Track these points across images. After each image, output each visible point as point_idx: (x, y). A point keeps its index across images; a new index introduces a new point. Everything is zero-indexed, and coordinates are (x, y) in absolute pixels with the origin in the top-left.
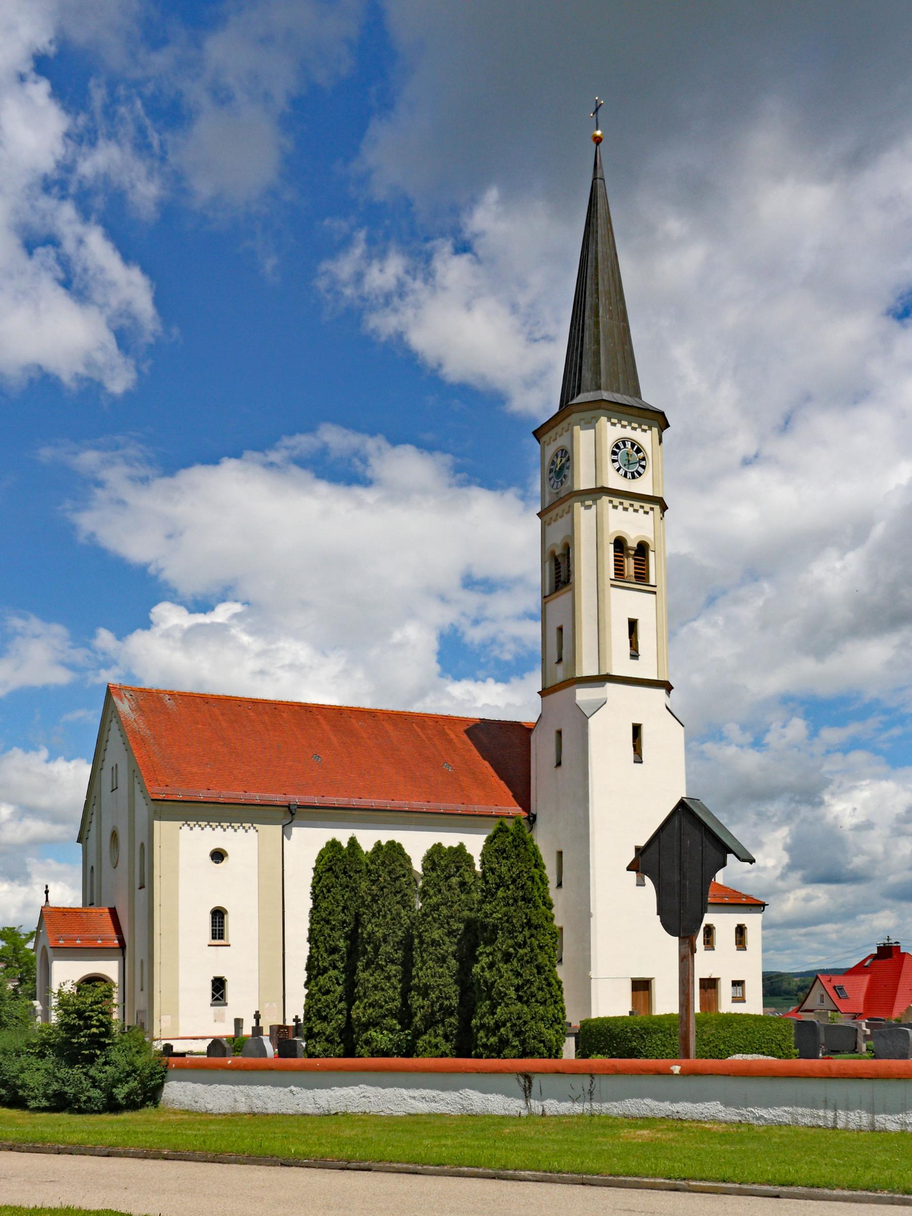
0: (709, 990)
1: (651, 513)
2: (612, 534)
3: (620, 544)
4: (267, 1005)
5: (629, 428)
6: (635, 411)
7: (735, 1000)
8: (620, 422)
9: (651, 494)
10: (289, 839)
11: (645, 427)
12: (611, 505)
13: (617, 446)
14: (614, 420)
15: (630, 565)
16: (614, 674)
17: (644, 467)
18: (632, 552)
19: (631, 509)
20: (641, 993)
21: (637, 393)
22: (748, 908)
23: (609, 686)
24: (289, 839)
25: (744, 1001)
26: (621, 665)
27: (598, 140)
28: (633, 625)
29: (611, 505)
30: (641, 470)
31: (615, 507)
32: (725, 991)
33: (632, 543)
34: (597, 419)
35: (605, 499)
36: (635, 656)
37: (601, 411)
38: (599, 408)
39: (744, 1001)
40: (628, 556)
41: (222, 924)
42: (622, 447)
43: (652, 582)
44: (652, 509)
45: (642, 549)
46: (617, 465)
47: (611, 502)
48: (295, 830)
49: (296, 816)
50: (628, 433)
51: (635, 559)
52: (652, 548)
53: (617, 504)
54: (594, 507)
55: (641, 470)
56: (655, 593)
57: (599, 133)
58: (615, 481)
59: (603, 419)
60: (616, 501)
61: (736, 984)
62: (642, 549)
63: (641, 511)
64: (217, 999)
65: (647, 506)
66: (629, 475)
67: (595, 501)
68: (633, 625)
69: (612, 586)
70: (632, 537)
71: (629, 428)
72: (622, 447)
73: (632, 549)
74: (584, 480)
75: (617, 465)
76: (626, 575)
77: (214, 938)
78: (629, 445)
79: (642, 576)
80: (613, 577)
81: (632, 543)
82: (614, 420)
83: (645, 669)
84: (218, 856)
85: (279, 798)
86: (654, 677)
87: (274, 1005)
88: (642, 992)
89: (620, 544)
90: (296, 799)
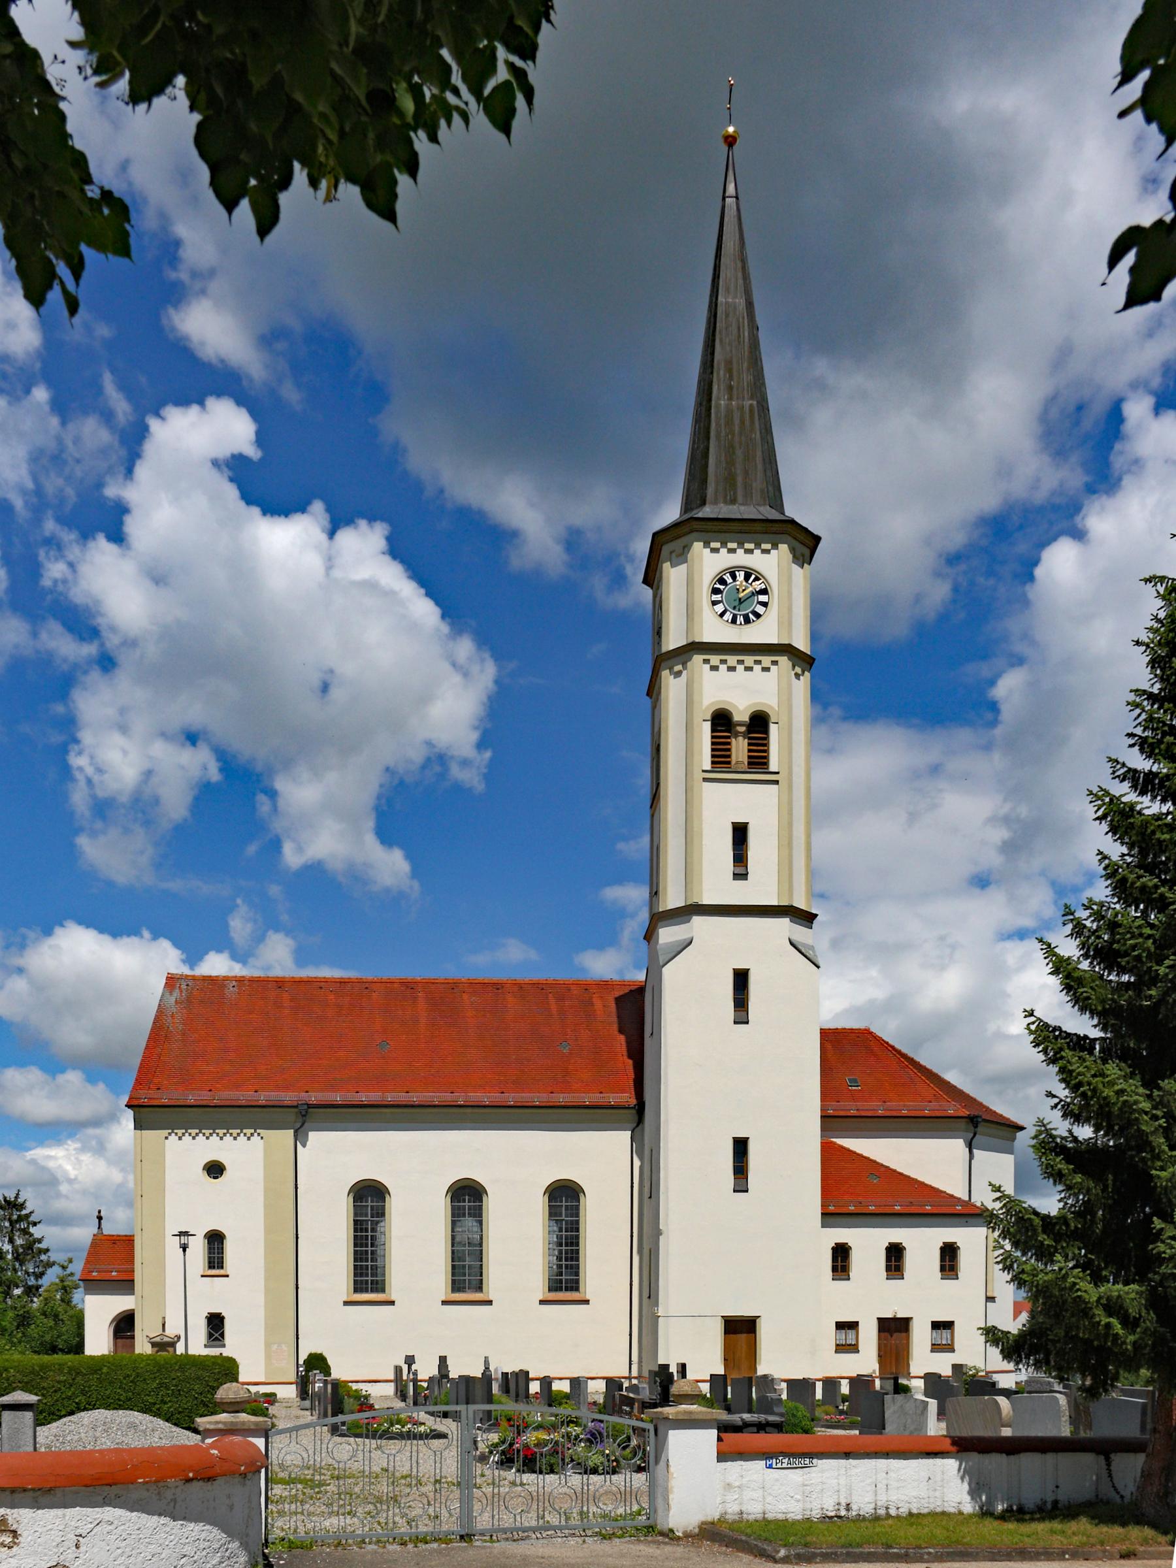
0: (895, 1335)
1: (774, 668)
2: (708, 708)
3: (721, 720)
4: (275, 1347)
5: (740, 552)
6: (758, 527)
7: (936, 1348)
8: (758, 546)
9: (776, 642)
10: (304, 1146)
11: (767, 546)
12: (708, 666)
13: (722, 581)
14: (764, 546)
15: (740, 748)
16: (705, 903)
17: (765, 604)
18: (742, 729)
19: (740, 668)
20: (743, 1337)
21: (776, 501)
22: (963, 1220)
23: (697, 920)
24: (304, 1146)
25: (953, 1351)
26: (718, 886)
27: (730, 141)
28: (740, 833)
29: (708, 666)
30: (760, 609)
31: (714, 668)
32: (921, 1336)
33: (741, 715)
34: (687, 548)
35: (698, 659)
36: (740, 876)
37: (695, 534)
38: (692, 531)
39: (953, 1351)
40: (736, 735)
41: (221, 1250)
42: (729, 580)
43: (773, 767)
44: (775, 663)
45: (759, 722)
46: (719, 608)
47: (706, 661)
48: (313, 1136)
49: (979, 1129)
50: (740, 558)
51: (749, 738)
52: (773, 719)
53: (717, 663)
54: (685, 672)
55: (760, 609)
56: (777, 782)
57: (731, 129)
58: (715, 630)
59: (698, 546)
60: (715, 659)
61: (936, 1325)
62: (759, 722)
63: (740, 668)
64: (216, 1339)
65: (766, 660)
66: (740, 619)
67: (684, 664)
68: (740, 833)
69: (705, 780)
70: (741, 708)
71: (740, 552)
72: (729, 580)
73: (741, 724)
74: (673, 640)
75: (719, 608)
76: (733, 762)
77: (211, 1267)
78: (741, 576)
79: (758, 761)
80: (708, 766)
81: (741, 715)
82: (714, 545)
83: (761, 888)
84: (215, 1169)
85: (289, 1097)
86: (774, 902)
87: (284, 1347)
88: (744, 1336)
89: (721, 720)
90: (314, 1098)
